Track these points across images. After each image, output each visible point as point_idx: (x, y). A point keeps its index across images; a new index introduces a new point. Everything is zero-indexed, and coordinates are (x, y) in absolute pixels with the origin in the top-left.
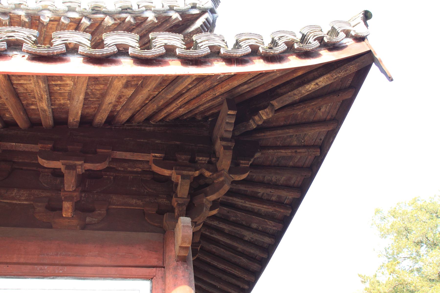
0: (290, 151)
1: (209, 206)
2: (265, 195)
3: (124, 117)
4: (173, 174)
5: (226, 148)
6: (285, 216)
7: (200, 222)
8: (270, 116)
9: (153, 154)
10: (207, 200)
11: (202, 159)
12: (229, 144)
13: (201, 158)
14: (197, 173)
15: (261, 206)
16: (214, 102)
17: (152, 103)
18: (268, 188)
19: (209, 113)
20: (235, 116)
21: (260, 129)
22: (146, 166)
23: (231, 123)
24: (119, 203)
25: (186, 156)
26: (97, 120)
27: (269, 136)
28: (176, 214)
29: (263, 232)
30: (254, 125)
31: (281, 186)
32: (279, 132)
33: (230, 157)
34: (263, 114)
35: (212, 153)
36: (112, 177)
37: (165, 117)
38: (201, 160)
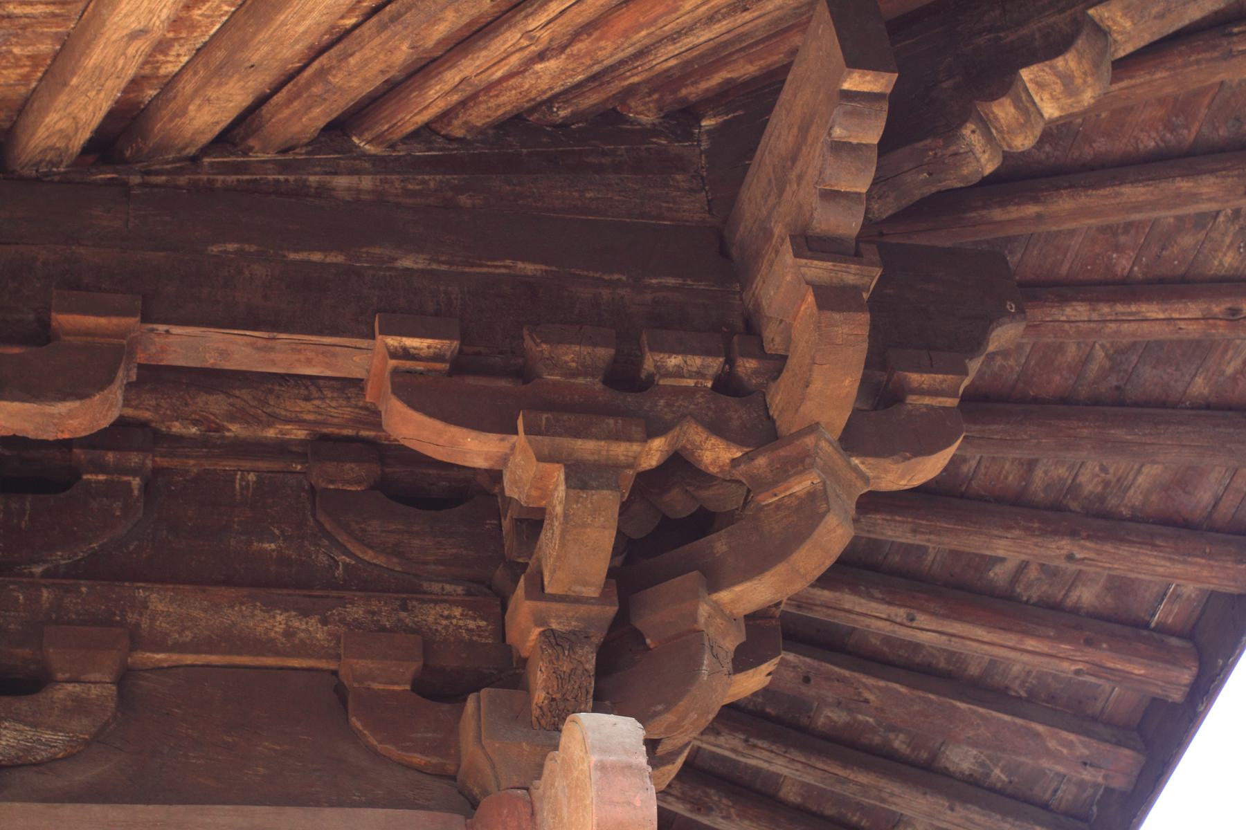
0: (1194, 309)
1: (730, 643)
2: (1033, 573)
3: (205, 113)
4: (518, 458)
5: (831, 298)
6: (1157, 704)
7: (680, 740)
8: (1088, 97)
9: (393, 341)
10: (718, 608)
11: (682, 366)
12: (850, 274)
13: (673, 361)
14: (654, 452)
15: (1011, 639)
16: (747, 16)
17: (383, 27)
18: (1055, 533)
19: (704, 85)
20: (885, 106)
21: (1018, 178)
22: (336, 414)
23: (859, 147)
24: (188, 635)
25: (585, 350)
26: (42, 133)
27: (1070, 223)
28: (539, 696)
29: (1014, 797)
30: (984, 158)
31: (1133, 519)
32: (1133, 192)
33: (858, 354)
34: (1041, 86)
35: (740, 331)
36: (136, 482)
37: (446, 116)
38: (678, 373)
